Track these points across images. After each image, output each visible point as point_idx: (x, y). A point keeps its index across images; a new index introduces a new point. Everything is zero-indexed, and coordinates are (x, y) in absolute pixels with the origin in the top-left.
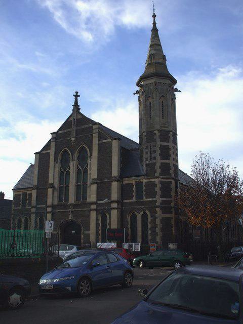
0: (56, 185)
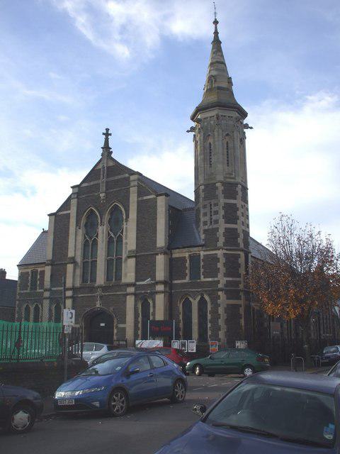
0: (79, 259)
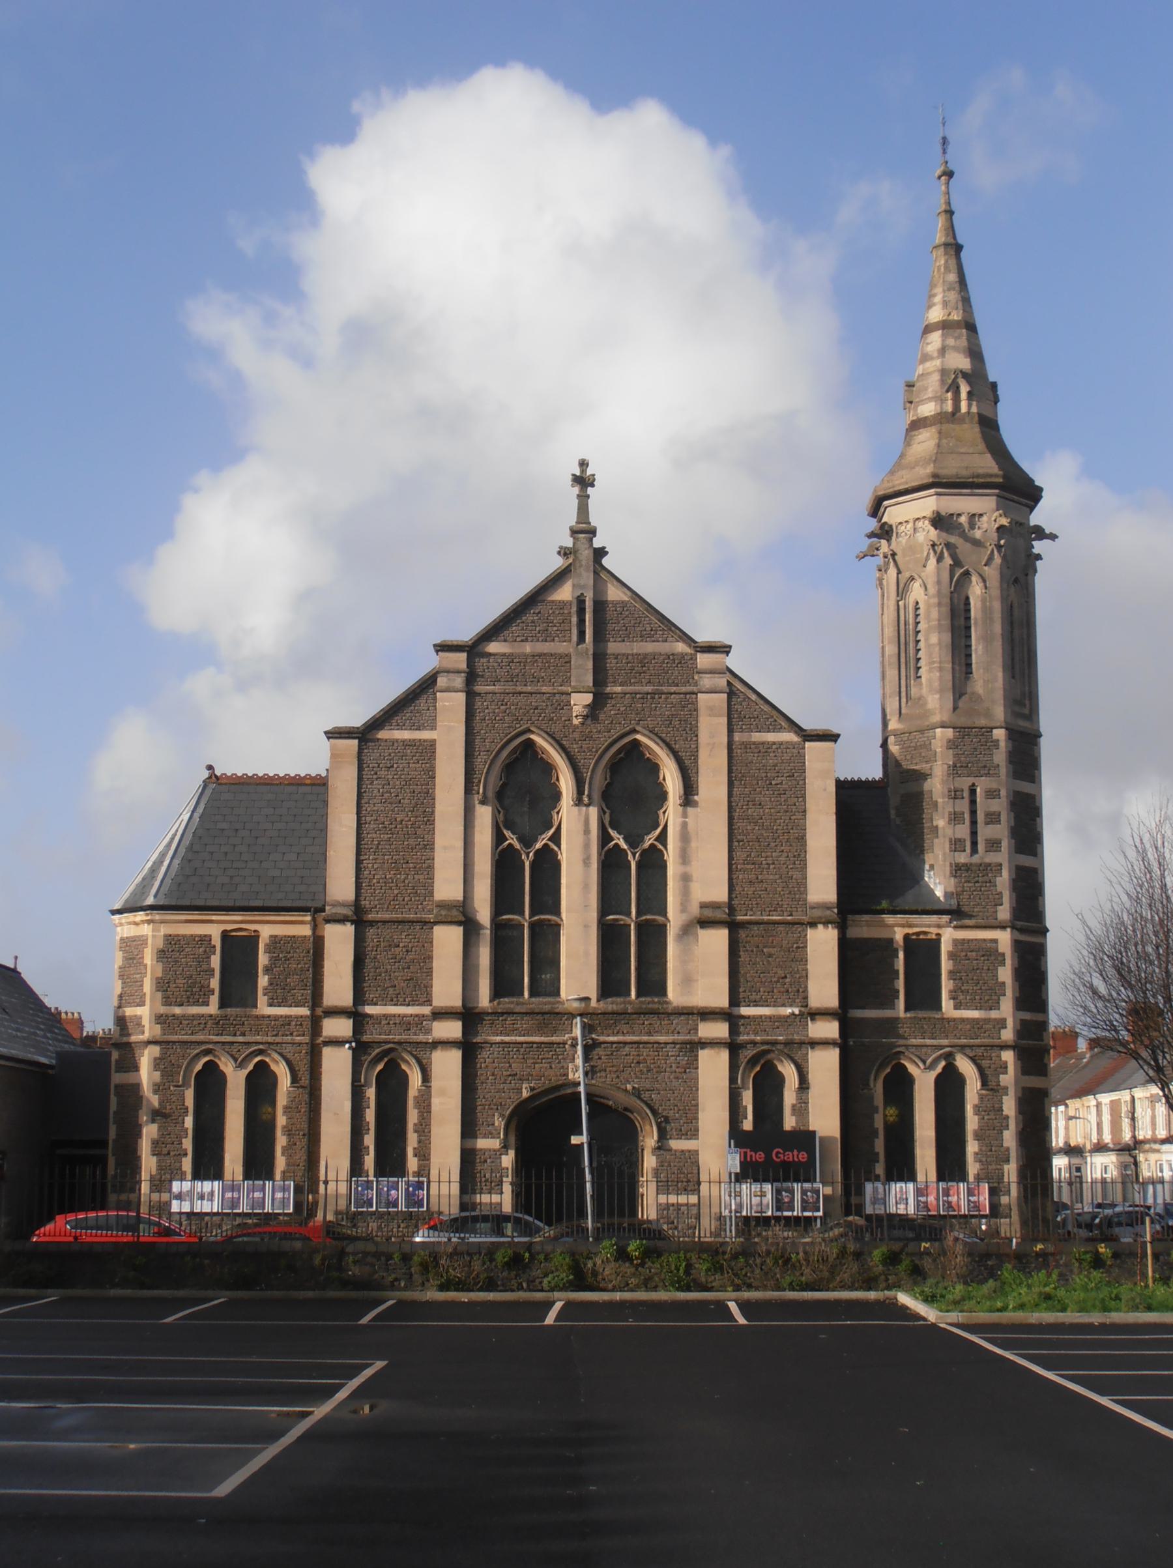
0: (484, 913)
